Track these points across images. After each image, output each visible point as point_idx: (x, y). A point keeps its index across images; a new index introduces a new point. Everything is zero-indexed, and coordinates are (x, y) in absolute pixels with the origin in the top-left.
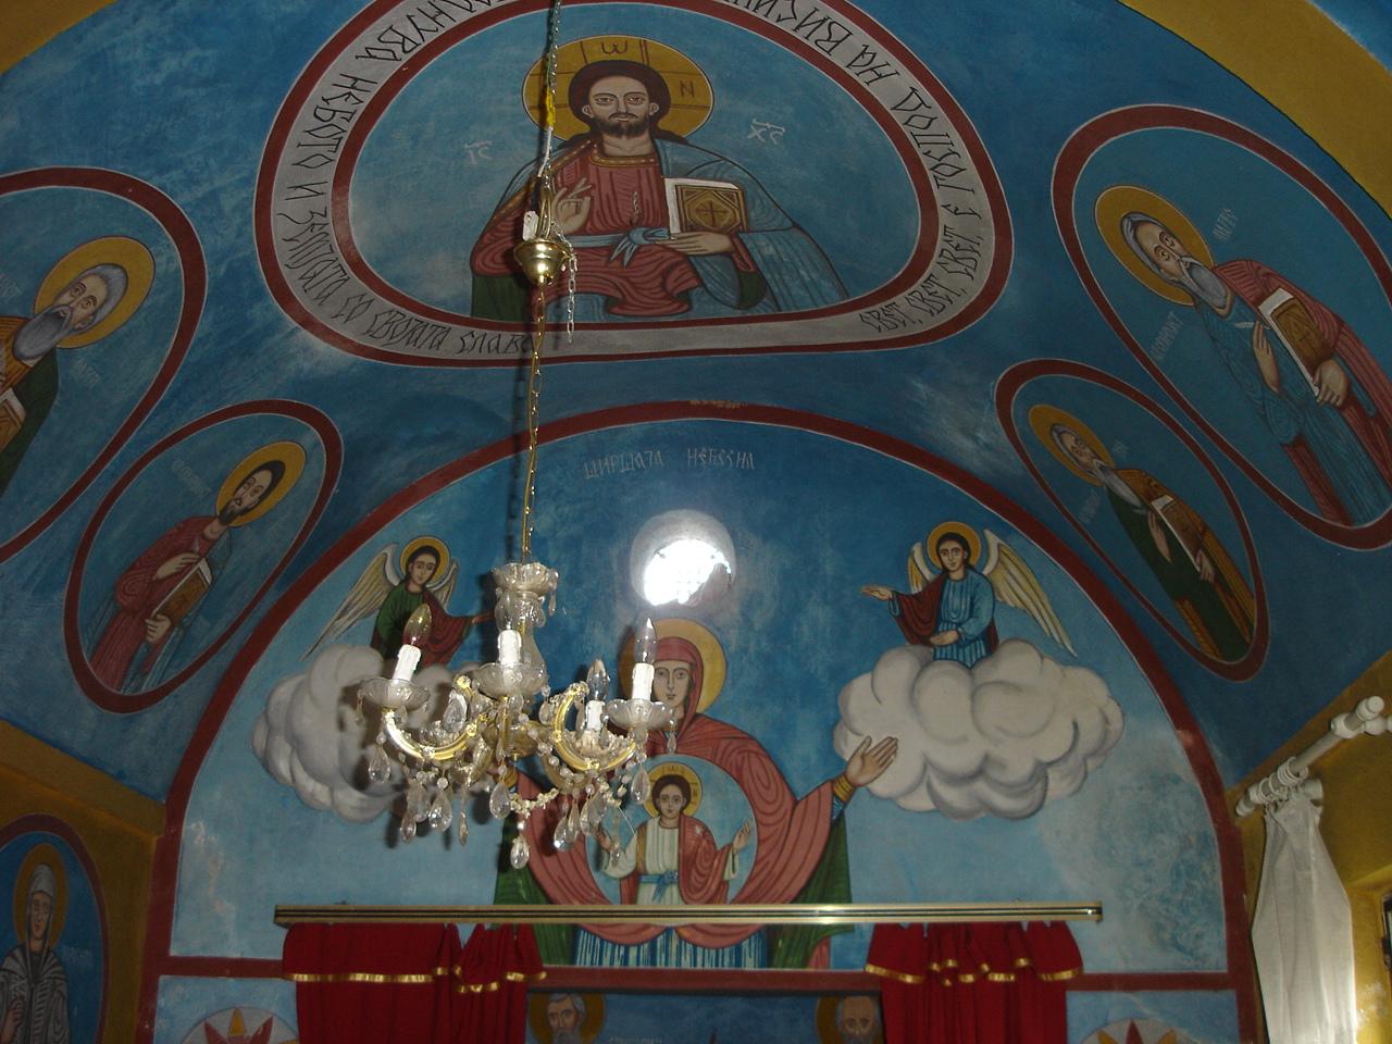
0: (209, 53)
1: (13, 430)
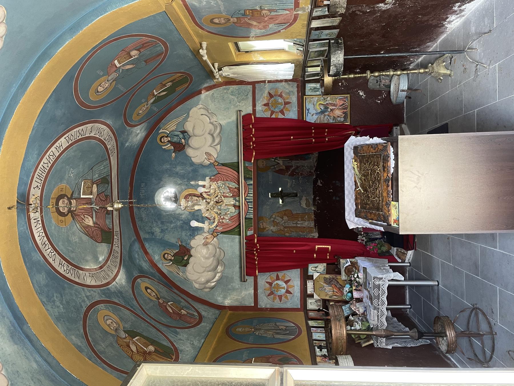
0: (55, 295)
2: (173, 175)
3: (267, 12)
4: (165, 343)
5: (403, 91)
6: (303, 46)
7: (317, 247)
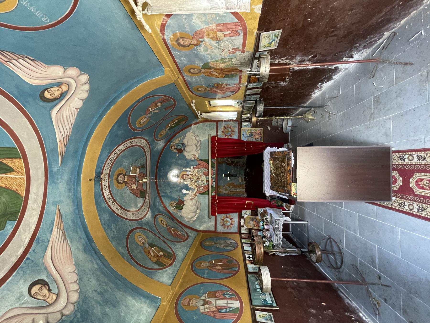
0: (113, 225)
1: (157, 248)
2: (177, 165)
4: (169, 250)
5: (289, 127)
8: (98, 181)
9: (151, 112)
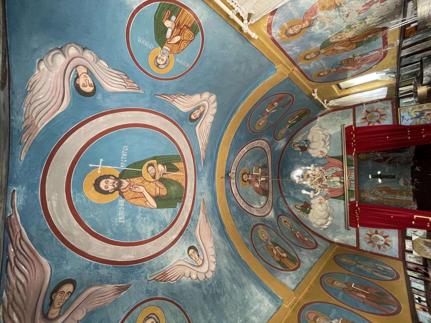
3: (359, 57)
4: (293, 254)
6: (395, 73)
7: (415, 216)
8: (228, 179)
9: (268, 113)
